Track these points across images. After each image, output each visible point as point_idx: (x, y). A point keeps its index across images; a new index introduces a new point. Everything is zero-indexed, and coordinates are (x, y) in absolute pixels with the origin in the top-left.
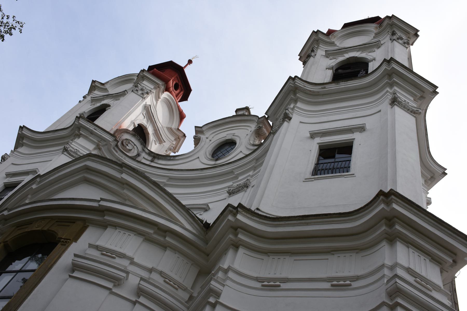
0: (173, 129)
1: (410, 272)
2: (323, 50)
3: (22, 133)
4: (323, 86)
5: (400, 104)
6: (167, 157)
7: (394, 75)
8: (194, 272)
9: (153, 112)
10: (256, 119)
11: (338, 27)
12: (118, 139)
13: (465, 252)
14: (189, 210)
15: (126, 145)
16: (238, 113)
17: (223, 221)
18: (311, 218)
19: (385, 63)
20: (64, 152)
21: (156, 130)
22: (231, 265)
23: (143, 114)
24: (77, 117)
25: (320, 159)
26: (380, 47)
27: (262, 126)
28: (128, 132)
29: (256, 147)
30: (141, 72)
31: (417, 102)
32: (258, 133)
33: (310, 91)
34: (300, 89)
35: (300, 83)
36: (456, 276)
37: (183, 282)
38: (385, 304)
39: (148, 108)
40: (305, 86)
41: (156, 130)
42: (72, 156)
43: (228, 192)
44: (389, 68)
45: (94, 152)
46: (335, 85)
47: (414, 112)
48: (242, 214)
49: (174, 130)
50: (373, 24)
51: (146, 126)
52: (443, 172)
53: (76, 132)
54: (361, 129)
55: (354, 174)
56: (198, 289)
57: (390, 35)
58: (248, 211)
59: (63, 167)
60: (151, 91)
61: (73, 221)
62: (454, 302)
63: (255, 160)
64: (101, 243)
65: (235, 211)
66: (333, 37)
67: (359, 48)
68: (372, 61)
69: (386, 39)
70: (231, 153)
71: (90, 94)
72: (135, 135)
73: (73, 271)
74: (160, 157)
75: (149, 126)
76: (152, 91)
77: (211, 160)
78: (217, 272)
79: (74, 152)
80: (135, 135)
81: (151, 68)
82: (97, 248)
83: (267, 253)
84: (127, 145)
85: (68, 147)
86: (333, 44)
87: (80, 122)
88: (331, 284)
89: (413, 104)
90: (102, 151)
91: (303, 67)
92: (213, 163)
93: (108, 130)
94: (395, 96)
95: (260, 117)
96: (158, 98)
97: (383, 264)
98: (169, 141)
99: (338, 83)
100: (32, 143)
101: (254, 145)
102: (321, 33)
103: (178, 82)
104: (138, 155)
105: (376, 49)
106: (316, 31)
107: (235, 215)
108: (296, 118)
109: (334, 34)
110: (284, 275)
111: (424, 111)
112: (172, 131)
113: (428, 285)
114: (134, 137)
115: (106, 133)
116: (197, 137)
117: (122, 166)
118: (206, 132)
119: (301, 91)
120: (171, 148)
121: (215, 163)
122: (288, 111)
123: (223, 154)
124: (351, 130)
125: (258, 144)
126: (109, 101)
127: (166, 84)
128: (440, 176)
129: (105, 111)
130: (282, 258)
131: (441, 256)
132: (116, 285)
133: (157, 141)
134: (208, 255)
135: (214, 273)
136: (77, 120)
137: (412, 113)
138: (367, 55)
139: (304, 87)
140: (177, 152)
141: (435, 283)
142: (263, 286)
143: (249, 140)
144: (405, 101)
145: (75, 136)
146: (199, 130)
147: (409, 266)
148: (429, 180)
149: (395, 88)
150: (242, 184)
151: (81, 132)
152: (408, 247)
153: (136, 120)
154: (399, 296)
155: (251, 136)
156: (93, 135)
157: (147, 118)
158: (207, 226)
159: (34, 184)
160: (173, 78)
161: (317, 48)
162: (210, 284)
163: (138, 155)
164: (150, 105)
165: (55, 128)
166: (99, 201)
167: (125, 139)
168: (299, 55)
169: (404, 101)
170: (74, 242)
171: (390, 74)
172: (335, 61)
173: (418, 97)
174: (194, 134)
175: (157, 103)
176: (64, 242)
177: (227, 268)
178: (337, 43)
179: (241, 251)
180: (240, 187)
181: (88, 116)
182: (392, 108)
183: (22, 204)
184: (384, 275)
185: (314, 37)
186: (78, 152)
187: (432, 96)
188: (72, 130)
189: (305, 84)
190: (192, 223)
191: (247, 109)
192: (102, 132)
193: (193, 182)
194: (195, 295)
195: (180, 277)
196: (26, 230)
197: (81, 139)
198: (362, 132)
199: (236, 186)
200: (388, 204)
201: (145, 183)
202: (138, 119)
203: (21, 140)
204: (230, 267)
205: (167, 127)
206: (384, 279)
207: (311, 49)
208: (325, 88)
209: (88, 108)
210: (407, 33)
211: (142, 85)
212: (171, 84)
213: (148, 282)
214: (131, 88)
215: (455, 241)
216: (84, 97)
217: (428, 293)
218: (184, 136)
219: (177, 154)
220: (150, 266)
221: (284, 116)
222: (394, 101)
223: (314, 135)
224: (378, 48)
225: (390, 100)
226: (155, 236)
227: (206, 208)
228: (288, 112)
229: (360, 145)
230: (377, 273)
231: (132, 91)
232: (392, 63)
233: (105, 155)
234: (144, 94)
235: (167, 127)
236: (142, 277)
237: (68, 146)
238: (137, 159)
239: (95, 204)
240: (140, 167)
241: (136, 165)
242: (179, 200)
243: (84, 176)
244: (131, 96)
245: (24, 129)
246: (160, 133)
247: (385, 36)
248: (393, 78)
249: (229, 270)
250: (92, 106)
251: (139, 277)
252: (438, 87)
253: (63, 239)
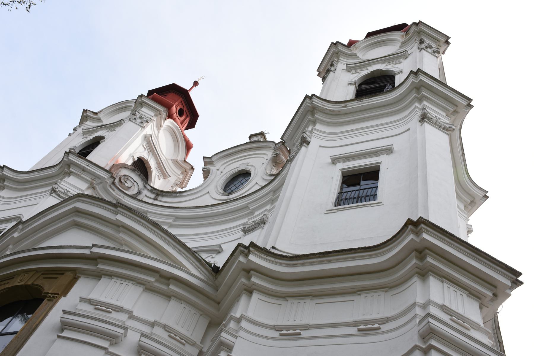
0: (179, 161)
1: (445, 310)
2: (343, 63)
3: (3, 173)
4: (344, 104)
5: (430, 121)
6: (172, 194)
7: (422, 88)
8: (204, 323)
9: (154, 143)
10: (272, 146)
11: (360, 36)
12: (115, 176)
13: (506, 284)
14: (195, 253)
15: (125, 182)
16: (251, 139)
17: (234, 263)
18: (333, 254)
19: (412, 75)
20: (52, 193)
21: (159, 163)
22: (244, 313)
23: (143, 146)
24: (66, 152)
25: (344, 187)
26: (407, 58)
27: (280, 153)
28: (126, 167)
29: (273, 178)
31: (450, 117)
32: (275, 161)
33: (330, 110)
34: (319, 109)
35: (318, 102)
36: (498, 311)
37: (191, 336)
38: (417, 347)
39: (148, 138)
40: (324, 106)
41: (159, 163)
42: (61, 197)
43: (243, 230)
44: (417, 81)
45: (87, 192)
46: (358, 102)
47: (447, 129)
48: (255, 254)
49: (180, 161)
50: (399, 32)
51: (148, 159)
52: (484, 195)
53: (66, 170)
54: (389, 150)
55: (381, 203)
56: (208, 343)
57: (417, 43)
58: (264, 251)
59: (49, 210)
60: (151, 118)
61: (61, 272)
62: (499, 341)
63: (272, 192)
64: (94, 296)
65: (246, 251)
66: (355, 48)
67: (384, 60)
68: (399, 73)
69: (413, 48)
70: (245, 186)
71: (82, 126)
72: (135, 170)
73: (62, 330)
74: (164, 194)
75: (151, 159)
76: (153, 118)
77: (223, 194)
78: (229, 322)
79: (64, 193)
80: (135, 170)
81: (151, 93)
82: (90, 301)
83: (285, 297)
84: (126, 182)
85: (56, 187)
86: (354, 56)
87: (69, 158)
88: (358, 329)
89: (445, 120)
90: (97, 190)
91: (323, 84)
92: (225, 197)
93: (103, 166)
94: (424, 112)
95: (276, 143)
96: (159, 126)
97: (414, 302)
98: (175, 175)
99: (361, 100)
100: (15, 185)
101: (271, 175)
102: (341, 45)
103: (182, 107)
104: (139, 193)
105: (403, 60)
106: (335, 43)
107: (246, 256)
108: (315, 142)
109: (356, 46)
110: (304, 322)
111: (459, 127)
112: (180, 166)
113: (465, 324)
114: (134, 172)
115: (100, 169)
116: (206, 168)
117: (117, 206)
118: (216, 163)
119: (320, 111)
120: (177, 183)
121: (228, 197)
122: (306, 134)
123: (237, 188)
124: (377, 153)
125: (276, 173)
126: (103, 132)
127: (168, 110)
128: (481, 199)
129: (99, 144)
130: (302, 302)
131: (480, 290)
132: (113, 344)
134: (219, 303)
135: (225, 323)
136: (66, 156)
137: (444, 130)
138: (393, 67)
139: (323, 106)
140: (185, 187)
141: (473, 321)
142: (281, 335)
143: (265, 169)
144: (436, 117)
145: (65, 174)
146: (208, 161)
147: (443, 303)
148: (469, 205)
149: (425, 103)
150: (259, 220)
151: (71, 169)
152: (442, 282)
153: (136, 153)
154: (432, 338)
155: (267, 165)
156: (85, 172)
157: (148, 150)
158: (216, 270)
159: (16, 232)
160: (177, 103)
161: (337, 61)
162: (221, 336)
163: (139, 193)
164: (151, 135)
165: (42, 166)
166: (91, 248)
167: (122, 175)
168: (317, 71)
169: (434, 118)
170: (63, 297)
171: (418, 87)
172: (358, 75)
173: (451, 112)
174: (203, 166)
175: (159, 132)
176: (51, 297)
177: (240, 317)
178: (360, 55)
179: (255, 296)
180: (256, 224)
181: (80, 151)
182: (421, 125)
183: (2, 256)
184: (416, 314)
185: (334, 49)
186: (69, 193)
187: (467, 110)
188: (61, 168)
189: (323, 103)
190: (199, 268)
191: (262, 134)
192: (95, 168)
193: (200, 221)
194: (205, 350)
195: (187, 330)
196: (7, 286)
197: (72, 177)
198: (389, 154)
199: (252, 222)
200: (418, 234)
201: (144, 224)
202: (137, 152)
203: (1, 182)
204: (243, 315)
205: (171, 160)
206: (416, 319)
207: (330, 63)
208: (346, 106)
209: (79, 141)
210: (436, 40)
211: (141, 112)
212: (175, 109)
213: (158, 342)
214: (129, 116)
215: (494, 271)
216: (74, 129)
217: (466, 333)
218: (192, 168)
219: (184, 189)
220: (152, 319)
221: (301, 140)
222: (424, 118)
223: (335, 160)
224: (405, 59)
225: (419, 117)
226: (157, 285)
227: (218, 251)
228: (306, 135)
229: (387, 168)
230: (408, 313)
231: (130, 120)
232: (420, 75)
233: (100, 195)
234: (143, 122)
235: (171, 160)
236: (143, 333)
237: (56, 186)
238: (137, 198)
239: (86, 252)
240: (142, 207)
241: (137, 205)
242: (183, 242)
243: (73, 220)
244: (128, 126)
245: (5, 169)
246: (164, 166)
247: (413, 45)
248: (422, 92)
249: (242, 319)
250: (84, 139)
251: (139, 333)
252: (472, 100)
253: (50, 294)
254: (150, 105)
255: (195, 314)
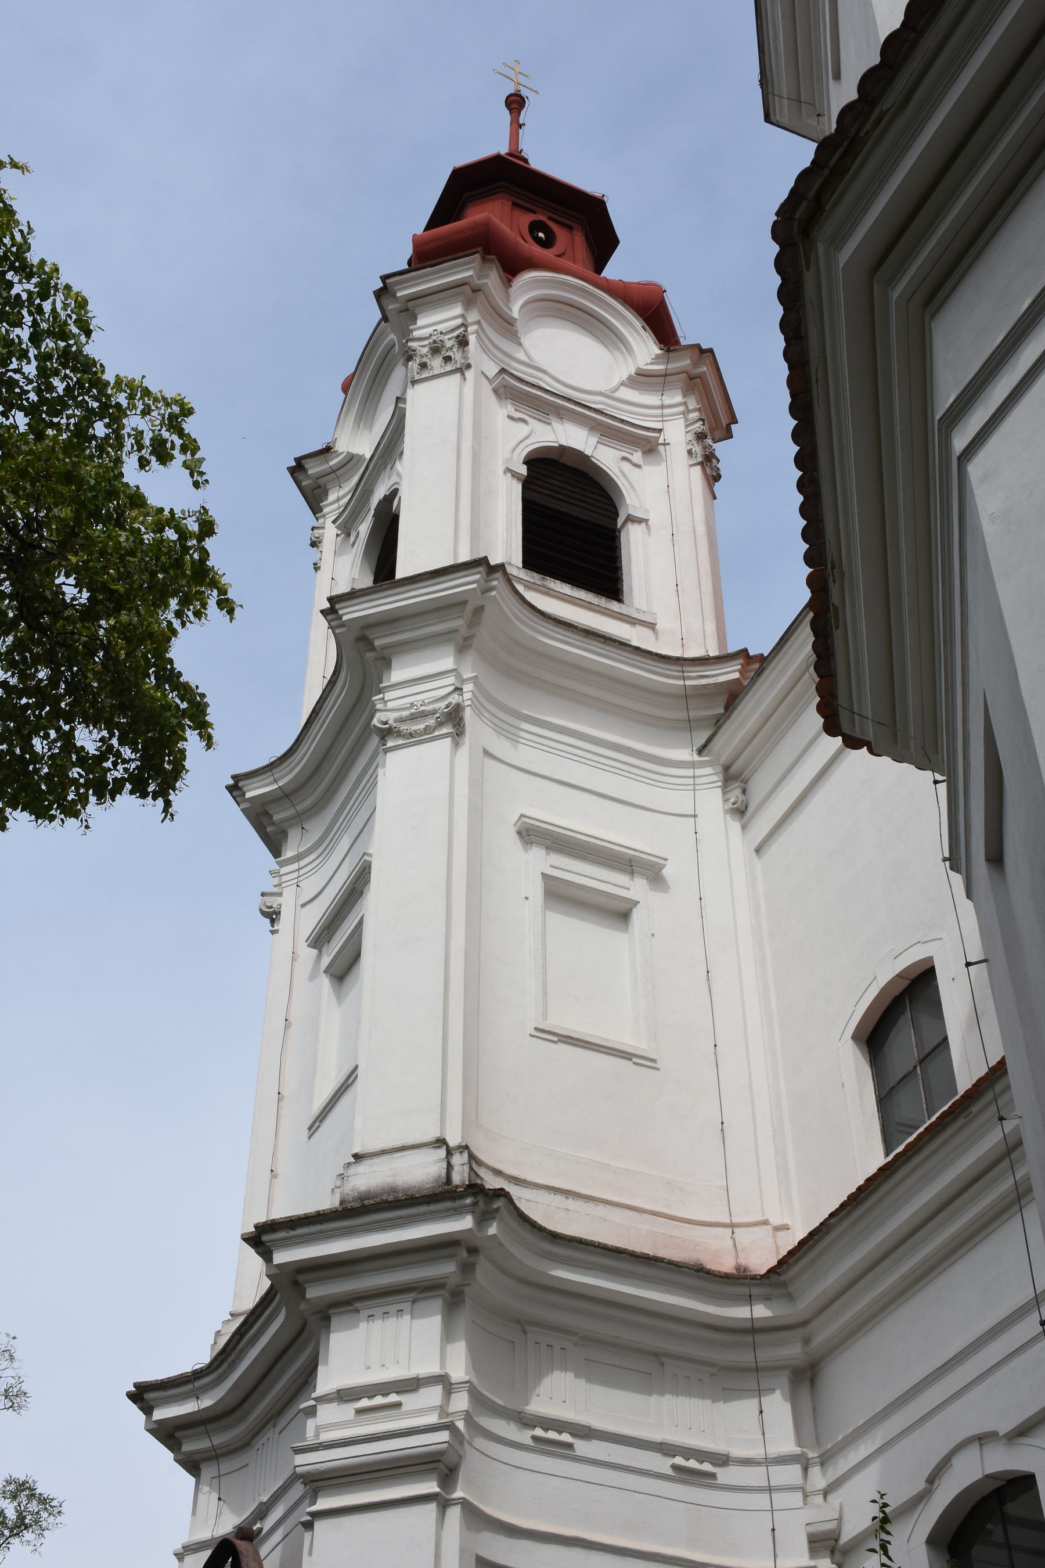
30: (382, 299)
83: (244, 1445)
96: (507, 327)
133: (632, 454)
254: (428, 292)
255: (400, 1311)
